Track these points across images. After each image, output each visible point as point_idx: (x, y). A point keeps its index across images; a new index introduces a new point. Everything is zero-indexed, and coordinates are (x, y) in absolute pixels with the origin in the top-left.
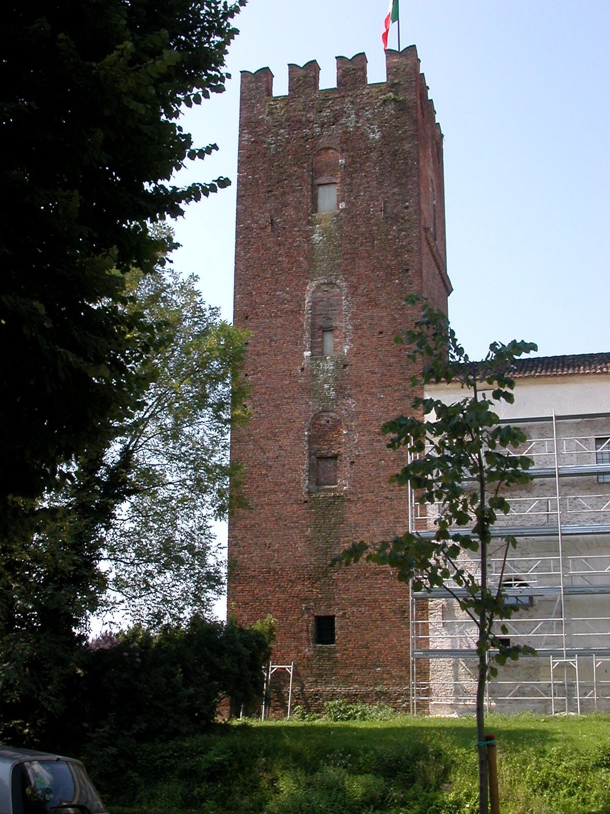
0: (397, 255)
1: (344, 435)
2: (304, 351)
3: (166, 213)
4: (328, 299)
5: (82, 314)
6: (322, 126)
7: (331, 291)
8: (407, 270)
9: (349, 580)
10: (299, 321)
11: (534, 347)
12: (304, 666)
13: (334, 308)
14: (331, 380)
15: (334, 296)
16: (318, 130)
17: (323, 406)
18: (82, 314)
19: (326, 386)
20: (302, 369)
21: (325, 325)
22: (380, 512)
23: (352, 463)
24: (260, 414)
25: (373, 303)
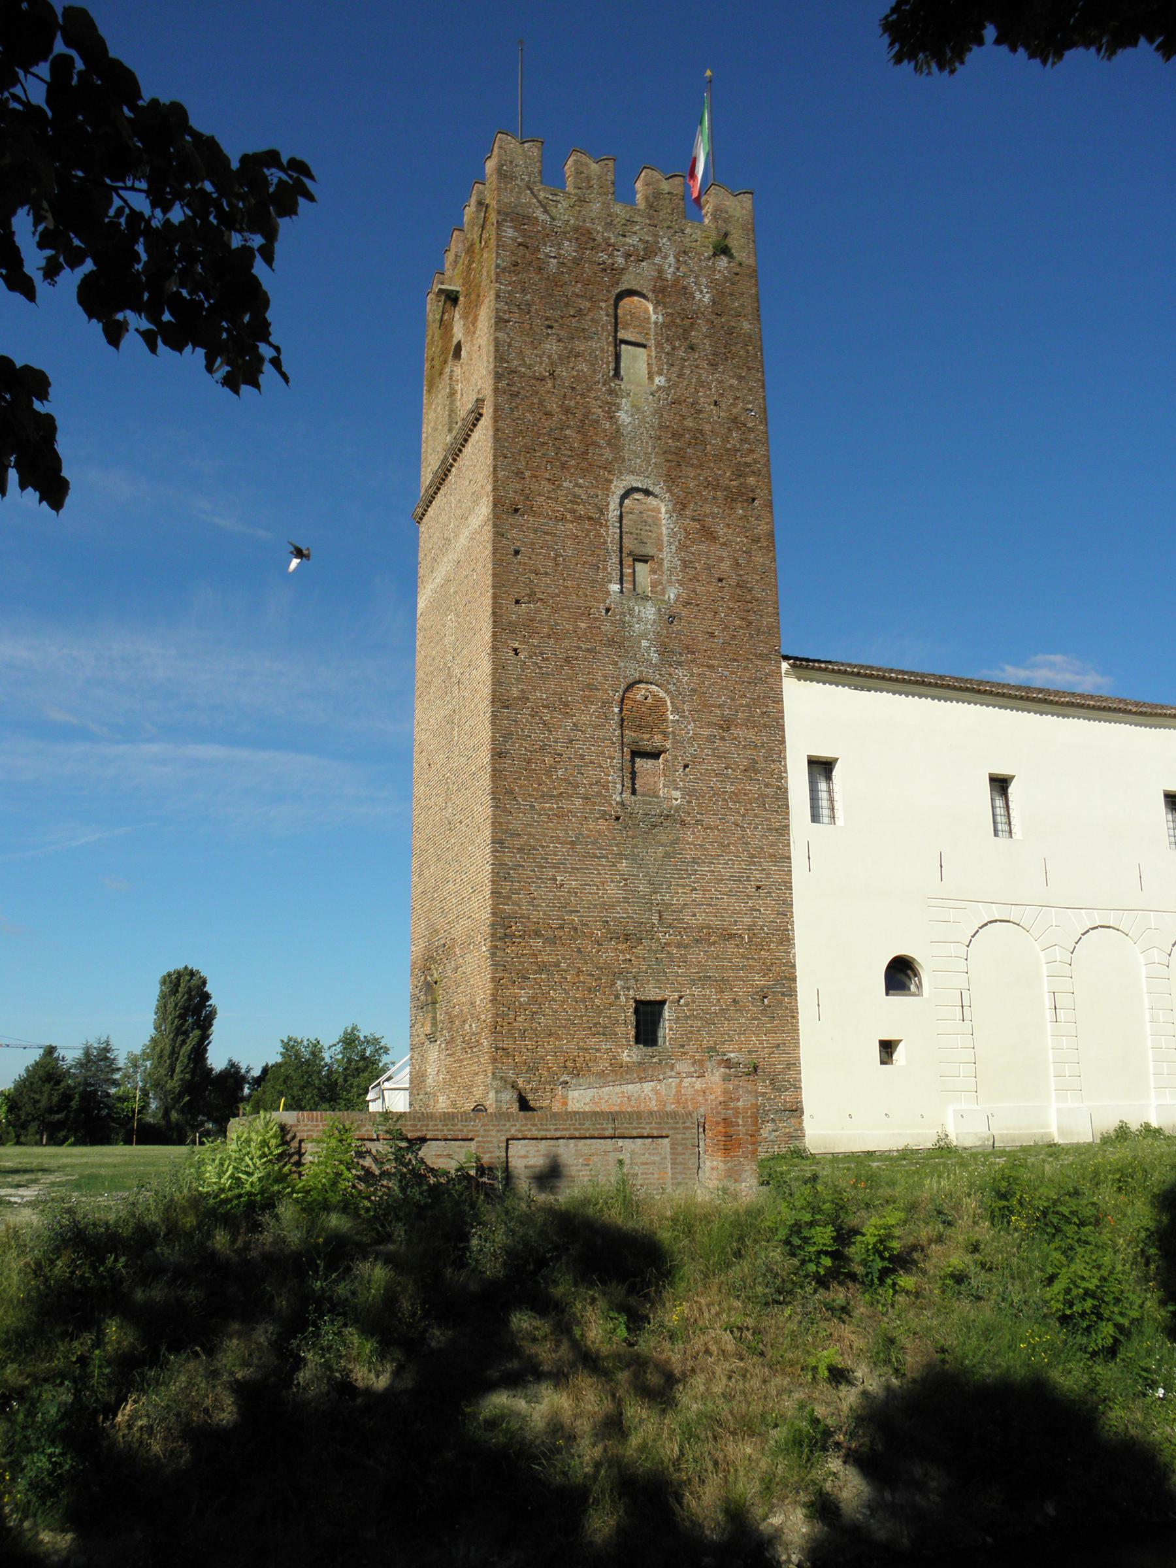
0: (739, 474)
1: (673, 721)
2: (610, 582)
3: (271, 190)
4: (641, 513)
5: (172, 150)
6: (628, 256)
7: (644, 501)
8: (754, 500)
9: (686, 947)
10: (600, 536)
11: (312, 178)
12: (803, 1480)
13: (648, 528)
14: (651, 636)
15: (649, 510)
16: (621, 260)
17: (641, 672)
18: (172, 150)
19: (644, 643)
20: (608, 610)
21: (637, 552)
22: (728, 845)
23: (686, 766)
24: (540, 668)
25: (709, 534)
